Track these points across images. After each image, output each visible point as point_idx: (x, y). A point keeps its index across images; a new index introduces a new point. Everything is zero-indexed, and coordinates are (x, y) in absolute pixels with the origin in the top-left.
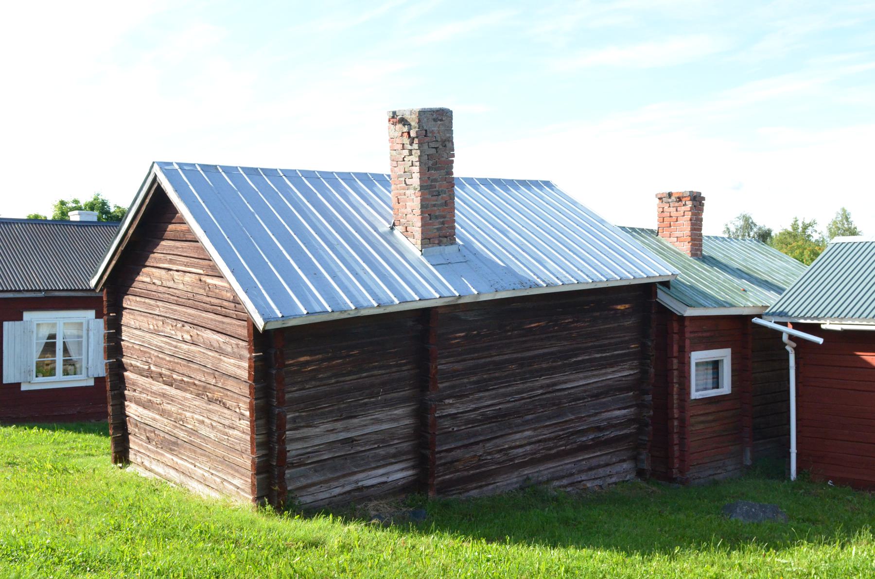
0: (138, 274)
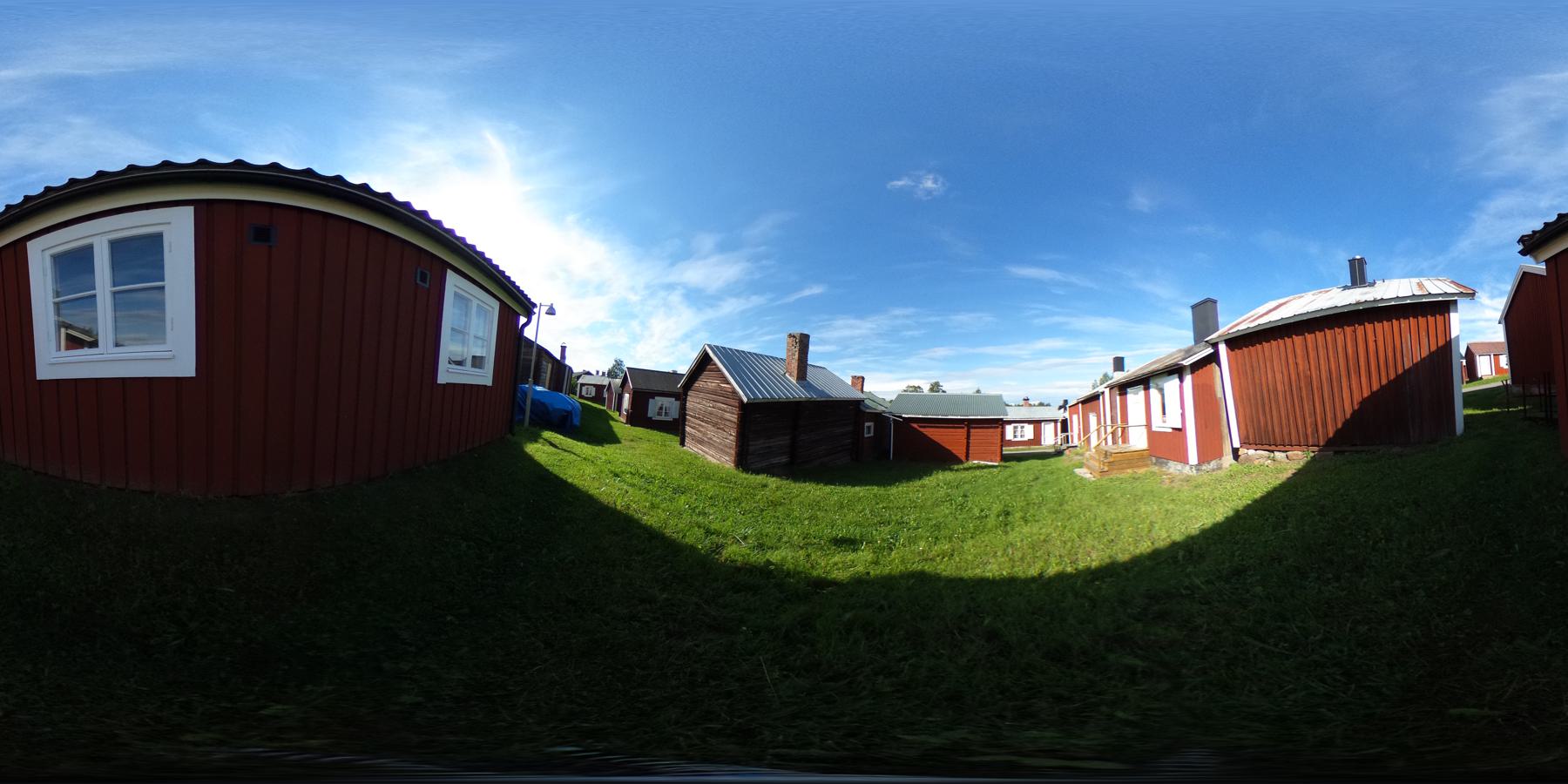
0: (696, 380)
